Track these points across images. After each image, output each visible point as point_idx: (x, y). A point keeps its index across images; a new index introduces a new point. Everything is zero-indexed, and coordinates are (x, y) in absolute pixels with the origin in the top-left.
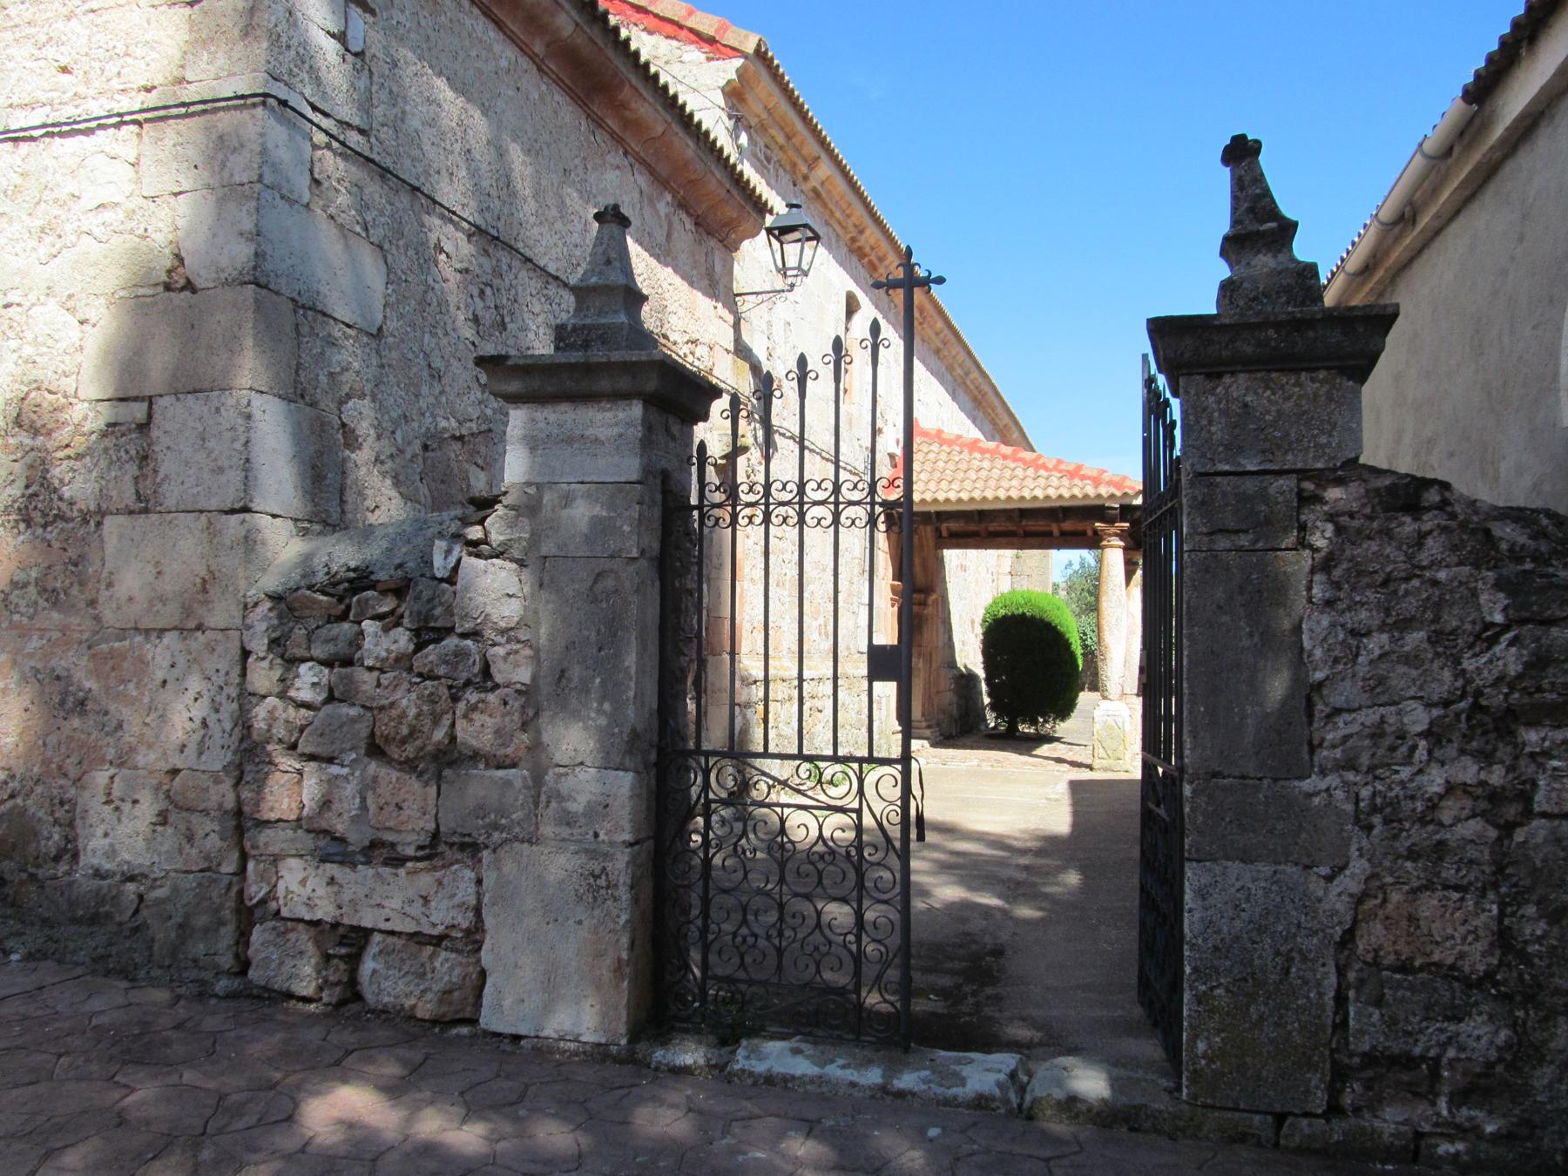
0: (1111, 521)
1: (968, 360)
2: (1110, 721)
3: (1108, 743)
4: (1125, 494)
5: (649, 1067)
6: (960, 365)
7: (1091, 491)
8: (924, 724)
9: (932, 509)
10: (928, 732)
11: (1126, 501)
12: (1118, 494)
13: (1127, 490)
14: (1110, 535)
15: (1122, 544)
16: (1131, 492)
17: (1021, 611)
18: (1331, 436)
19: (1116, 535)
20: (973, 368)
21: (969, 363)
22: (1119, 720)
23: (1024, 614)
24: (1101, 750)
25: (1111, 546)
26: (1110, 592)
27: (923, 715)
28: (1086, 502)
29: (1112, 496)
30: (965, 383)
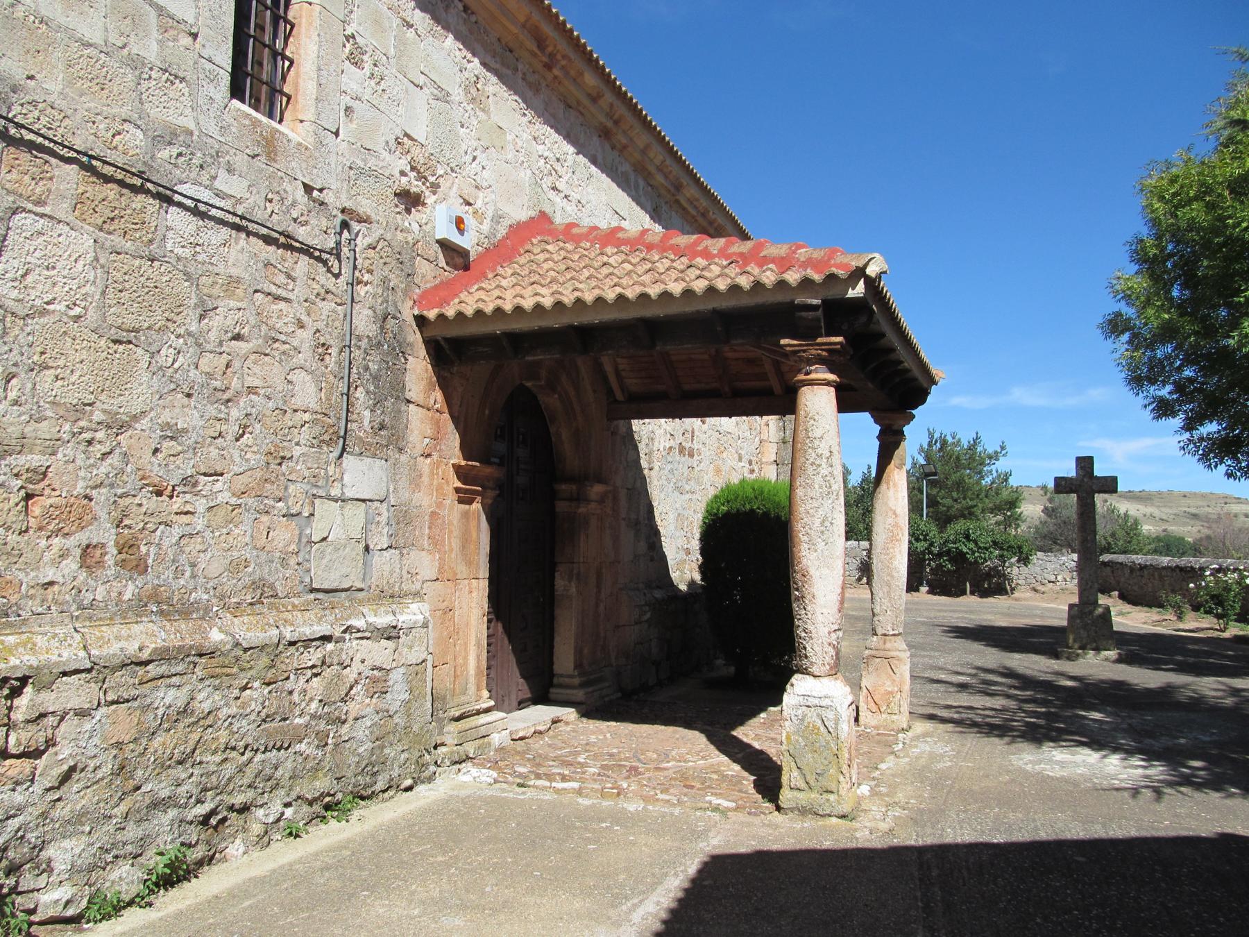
0: (809, 333)
1: (669, 161)
2: (812, 716)
3: (808, 759)
4: (832, 277)
5: (1135, 336)
6: (659, 169)
7: (769, 278)
8: (576, 681)
9: (498, 328)
10: (580, 695)
11: (833, 293)
12: (817, 277)
13: (834, 270)
14: (810, 362)
15: (832, 377)
16: (841, 273)
17: (748, 507)
18: (1214, 167)
19: (820, 360)
20: (685, 180)
21: (675, 170)
22: (830, 715)
23: (752, 511)
24: (795, 773)
25: (812, 383)
26: (810, 470)
27: (578, 665)
28: (759, 300)
29: (806, 283)
30: (677, 202)
